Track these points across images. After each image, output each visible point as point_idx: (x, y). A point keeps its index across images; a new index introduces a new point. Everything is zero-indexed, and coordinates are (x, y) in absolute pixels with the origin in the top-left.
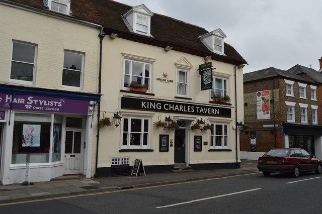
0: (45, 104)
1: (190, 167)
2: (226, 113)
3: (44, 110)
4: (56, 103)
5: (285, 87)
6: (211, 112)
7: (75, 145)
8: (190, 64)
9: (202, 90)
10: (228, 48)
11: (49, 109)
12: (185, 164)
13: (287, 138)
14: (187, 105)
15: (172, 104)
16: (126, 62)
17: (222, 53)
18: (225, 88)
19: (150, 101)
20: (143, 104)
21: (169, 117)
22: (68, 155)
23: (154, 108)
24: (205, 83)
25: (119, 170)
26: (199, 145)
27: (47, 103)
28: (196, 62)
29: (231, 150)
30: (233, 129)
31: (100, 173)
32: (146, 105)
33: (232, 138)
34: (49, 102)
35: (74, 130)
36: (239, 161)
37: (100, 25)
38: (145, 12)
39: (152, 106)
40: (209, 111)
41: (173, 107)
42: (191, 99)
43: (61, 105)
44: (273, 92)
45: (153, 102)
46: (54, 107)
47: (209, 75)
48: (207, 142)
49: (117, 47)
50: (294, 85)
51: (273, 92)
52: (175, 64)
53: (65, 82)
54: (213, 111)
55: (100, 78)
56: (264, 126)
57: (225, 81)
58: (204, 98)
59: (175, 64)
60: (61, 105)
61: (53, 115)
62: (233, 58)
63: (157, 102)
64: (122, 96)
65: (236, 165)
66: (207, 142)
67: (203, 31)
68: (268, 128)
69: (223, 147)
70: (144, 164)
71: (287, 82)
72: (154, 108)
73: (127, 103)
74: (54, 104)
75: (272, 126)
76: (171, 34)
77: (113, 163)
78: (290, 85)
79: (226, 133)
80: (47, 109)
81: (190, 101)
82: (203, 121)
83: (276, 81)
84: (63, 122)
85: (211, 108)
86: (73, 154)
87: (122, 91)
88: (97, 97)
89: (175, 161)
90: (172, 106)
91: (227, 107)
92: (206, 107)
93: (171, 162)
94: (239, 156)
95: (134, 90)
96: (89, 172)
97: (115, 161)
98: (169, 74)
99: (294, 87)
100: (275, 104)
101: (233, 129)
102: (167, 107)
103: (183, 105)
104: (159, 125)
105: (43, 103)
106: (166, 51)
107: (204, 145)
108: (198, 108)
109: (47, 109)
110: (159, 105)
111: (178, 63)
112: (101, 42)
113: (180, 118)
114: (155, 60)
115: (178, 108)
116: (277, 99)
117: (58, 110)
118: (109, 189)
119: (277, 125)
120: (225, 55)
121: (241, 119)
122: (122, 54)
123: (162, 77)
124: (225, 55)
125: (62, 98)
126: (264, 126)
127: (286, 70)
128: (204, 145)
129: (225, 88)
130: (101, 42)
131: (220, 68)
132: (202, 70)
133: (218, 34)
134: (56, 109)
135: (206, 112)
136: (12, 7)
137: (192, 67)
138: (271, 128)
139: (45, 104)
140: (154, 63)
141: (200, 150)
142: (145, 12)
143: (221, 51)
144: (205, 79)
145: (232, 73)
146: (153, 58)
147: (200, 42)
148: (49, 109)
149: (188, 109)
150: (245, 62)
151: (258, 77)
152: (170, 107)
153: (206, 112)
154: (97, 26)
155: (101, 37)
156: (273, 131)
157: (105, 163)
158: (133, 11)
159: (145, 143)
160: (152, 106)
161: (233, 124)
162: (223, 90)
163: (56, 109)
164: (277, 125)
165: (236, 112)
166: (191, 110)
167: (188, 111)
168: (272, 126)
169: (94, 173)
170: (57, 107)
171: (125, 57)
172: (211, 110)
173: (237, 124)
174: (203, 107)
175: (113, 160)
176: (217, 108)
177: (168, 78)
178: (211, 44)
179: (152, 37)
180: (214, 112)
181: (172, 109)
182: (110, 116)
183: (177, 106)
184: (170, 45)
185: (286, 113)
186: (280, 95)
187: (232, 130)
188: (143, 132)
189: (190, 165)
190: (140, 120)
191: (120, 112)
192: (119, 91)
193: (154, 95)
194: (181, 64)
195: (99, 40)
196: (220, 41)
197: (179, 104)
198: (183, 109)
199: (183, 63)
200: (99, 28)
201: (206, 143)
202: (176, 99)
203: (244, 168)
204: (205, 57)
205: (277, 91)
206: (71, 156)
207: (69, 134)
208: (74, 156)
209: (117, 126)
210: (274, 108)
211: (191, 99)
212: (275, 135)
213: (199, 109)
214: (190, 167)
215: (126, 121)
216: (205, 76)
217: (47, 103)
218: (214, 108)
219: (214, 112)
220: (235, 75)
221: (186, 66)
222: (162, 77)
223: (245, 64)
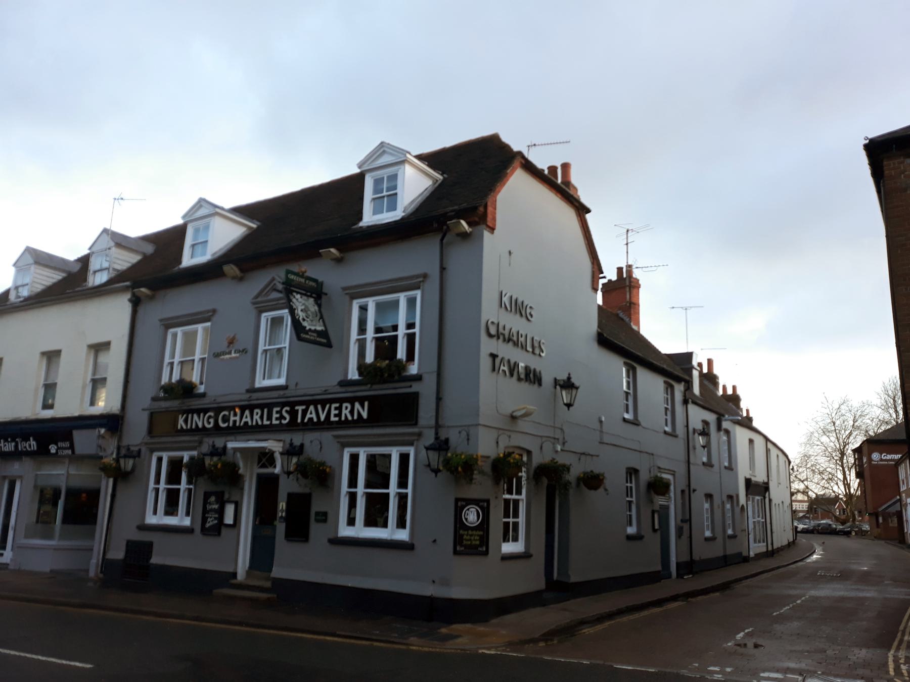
26: (209, 507)
39: (363, 407)
40: (333, 412)
41: (238, 418)
53: (317, 514)
85: (341, 401)
91: (403, 389)
108: (300, 408)
118: (175, 349)
128: (51, 407)
135: (323, 418)
149: (275, 415)
152: (232, 418)
153: (323, 418)
160: (363, 407)
166: (282, 417)
172: (339, 409)
180: (352, 412)
181: (235, 422)
198: (262, 417)
219: (352, 412)
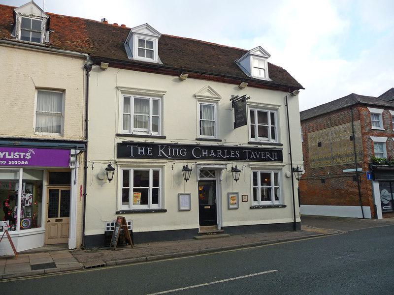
0: (7, 156)
1: (223, 230)
2: (277, 155)
3: (7, 164)
4: (22, 154)
5: (370, 118)
7: (60, 207)
8: (218, 95)
10: (273, 69)
11: (13, 162)
12: (217, 227)
13: (376, 186)
16: (125, 98)
18: (273, 123)
21: (236, 167)
22: (53, 220)
25: (118, 237)
27: (10, 155)
29: (284, 206)
30: (287, 177)
31: (89, 242)
33: (287, 191)
34: (12, 153)
35: (60, 188)
36: (298, 220)
37: (86, 53)
38: (150, 33)
41: (143, 151)
42: (221, 141)
43: (30, 157)
44: (353, 125)
46: (20, 159)
49: (110, 83)
50: (383, 114)
51: (353, 125)
52: (195, 96)
56: (344, 171)
57: (272, 114)
59: (195, 96)
60: (30, 157)
61: (21, 170)
62: (283, 83)
65: (294, 226)
67: (242, 53)
68: (350, 173)
70: (133, 231)
71: (372, 110)
73: (125, 150)
74: (20, 156)
75: (354, 170)
76: (185, 58)
77: (108, 229)
78: (377, 115)
79: (276, 183)
80: (10, 162)
82: (238, 168)
83: (355, 111)
84: (44, 179)
86: (59, 218)
87: (118, 135)
88: (82, 146)
89: (201, 224)
94: (297, 214)
96: (74, 242)
97: (110, 226)
98: (183, 108)
99: (383, 116)
100: (356, 141)
101: (287, 177)
105: (5, 156)
106: (182, 80)
109: (10, 162)
111: (200, 94)
112: (88, 75)
113: (203, 166)
116: (358, 135)
117: (27, 163)
119: (360, 169)
121: (298, 161)
122: (117, 88)
125: (30, 148)
126: (344, 171)
127: (377, 96)
129: (273, 123)
130: (88, 75)
131: (258, 98)
133: (259, 53)
134: (23, 163)
136: (6, 46)
137: (220, 99)
138: (353, 173)
139: (7, 156)
142: (150, 33)
143: (151, 57)
146: (279, 104)
147: (236, 66)
148: (13, 162)
150: (300, 87)
151: (334, 108)
155: (87, 69)
156: (356, 177)
157: (96, 229)
158: (132, 33)
159: (155, 201)
161: (287, 171)
162: (270, 125)
163: (23, 163)
164: (360, 169)
166: (235, 154)
168: (354, 170)
169: (80, 242)
170: (25, 160)
171: (123, 92)
175: (108, 225)
178: (258, 71)
179: (271, 80)
184: (106, 60)
185: (373, 152)
186: (363, 129)
189: (222, 228)
190: (147, 172)
191: (116, 163)
192: (115, 134)
193: (164, 138)
194: (203, 95)
195: (85, 72)
199: (207, 94)
200: (84, 58)
202: (198, 142)
203: (306, 229)
204: (239, 84)
205: (357, 123)
206: (57, 221)
207: (53, 194)
208: (61, 220)
209: (110, 180)
210: (355, 146)
211: (221, 141)
212: (359, 182)
214: (223, 230)
215: (126, 174)
217: (10, 155)
220: (287, 105)
221: (210, 97)
223: (300, 90)
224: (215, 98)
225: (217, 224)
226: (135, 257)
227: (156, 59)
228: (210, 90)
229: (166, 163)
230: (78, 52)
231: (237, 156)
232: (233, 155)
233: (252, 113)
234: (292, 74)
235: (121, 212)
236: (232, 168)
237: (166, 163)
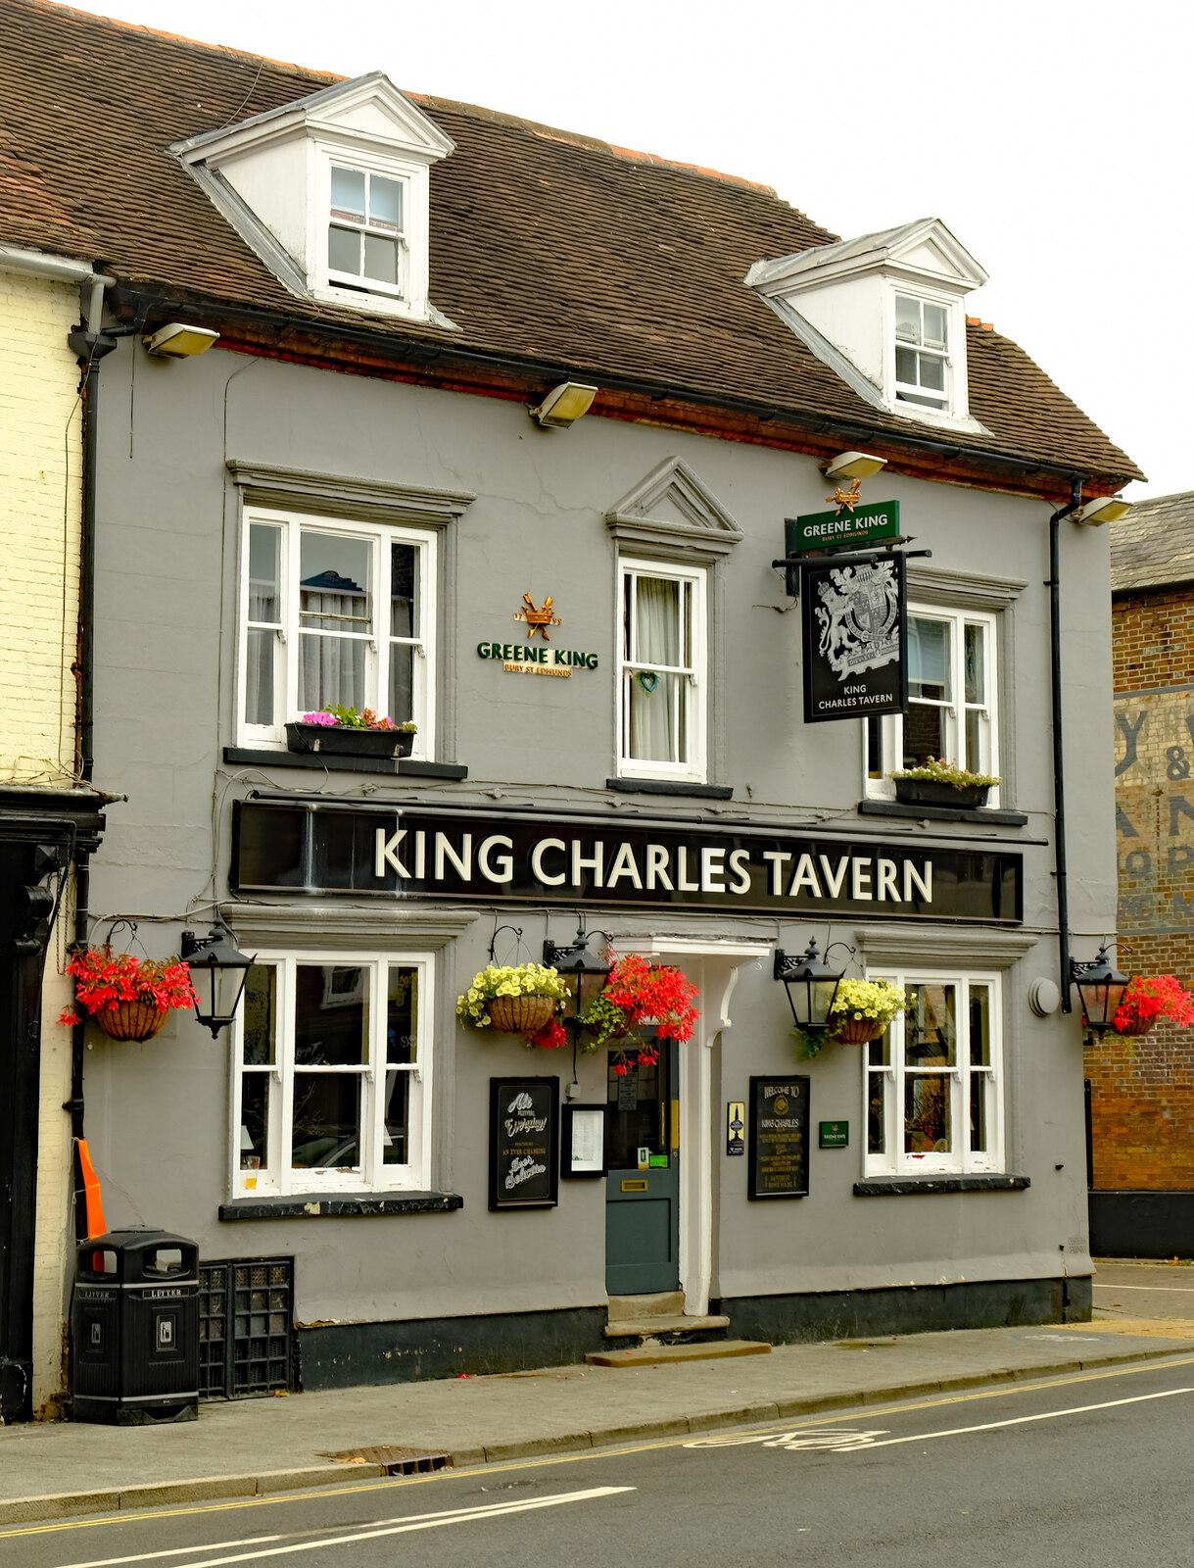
6: (873, 887)
9: (808, 719)
14: (695, 841)
15: (588, 835)
17: (953, 413)
19: (432, 824)
20: (385, 851)
23: (466, 874)
24: (843, 666)
28: (764, 497)
30: (1040, 1013)
32: (406, 852)
40: (859, 878)
41: (597, 863)
45: (455, 828)
47: (877, 603)
48: (843, 1126)
52: (611, 525)
54: (886, 881)
55: (83, 670)
58: (831, 777)
63: (481, 828)
64: (243, 795)
66: (843, 1126)
67: (784, 229)
69: (955, 1160)
72: (466, 874)
81: (719, 806)
90: (587, 853)
92: (836, 850)
93: (581, 1285)
95: (70, 818)
102: (557, 862)
103: (671, 839)
104: (489, 1021)
107: (823, 1144)
108: (778, 858)
110: (497, 850)
111: (633, 517)
112: (87, 391)
114: (466, 501)
115: (633, 871)
120: (974, 427)
122: (232, 469)
123: (515, 634)
124: (974, 427)
131: (956, 536)
132: (808, 563)
137: (732, 542)
140: (461, 529)
141: (799, 1185)
144: (835, 634)
145: (1033, 574)
149: (708, 869)
152: (578, 863)
154: (67, 274)
155: (87, 353)
165: (1060, 874)
166: (729, 876)
167: (708, 886)
172: (872, 870)
173: (1068, 972)
174: (816, 848)
176: (919, 856)
177: (563, 639)
180: (900, 882)
182: (155, 948)
183: (626, 850)
187: (1030, 1019)
188: (377, 1065)
196: (937, 316)
197: (641, 840)
198: (672, 870)
200: (81, 289)
201: (836, 1135)
202: (618, 799)
204: (537, 399)
213: (790, 870)
216: (836, 606)
218: (898, 854)
219: (900, 882)
220: (1053, 583)
222: (515, 634)
224: (708, 538)
225: (676, 1286)
226: (705, 1411)
227: (406, 296)
228: (683, 489)
229: (463, 923)
230: (73, 256)
231: (740, 881)
232: (715, 878)
233: (628, 578)
234: (1082, 404)
235: (315, 1209)
236: (780, 959)
237: (463, 923)
